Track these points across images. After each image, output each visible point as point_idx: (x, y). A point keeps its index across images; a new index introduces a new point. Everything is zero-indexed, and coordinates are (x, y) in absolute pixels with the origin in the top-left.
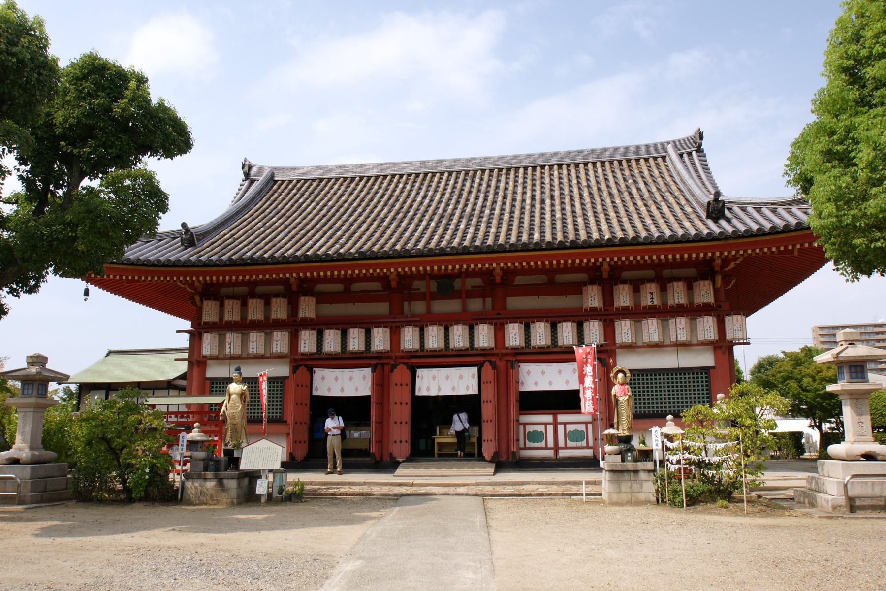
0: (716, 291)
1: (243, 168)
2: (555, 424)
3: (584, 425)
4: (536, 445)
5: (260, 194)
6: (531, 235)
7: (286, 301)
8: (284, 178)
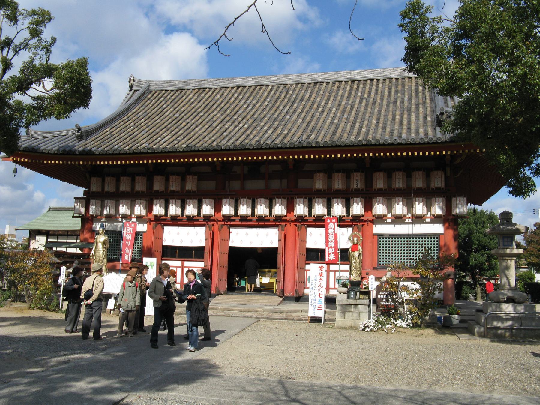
0: (446, 177)
1: (129, 82)
3: (330, 273)
5: (138, 99)
6: (417, 132)
7: (146, 178)
8: (156, 89)
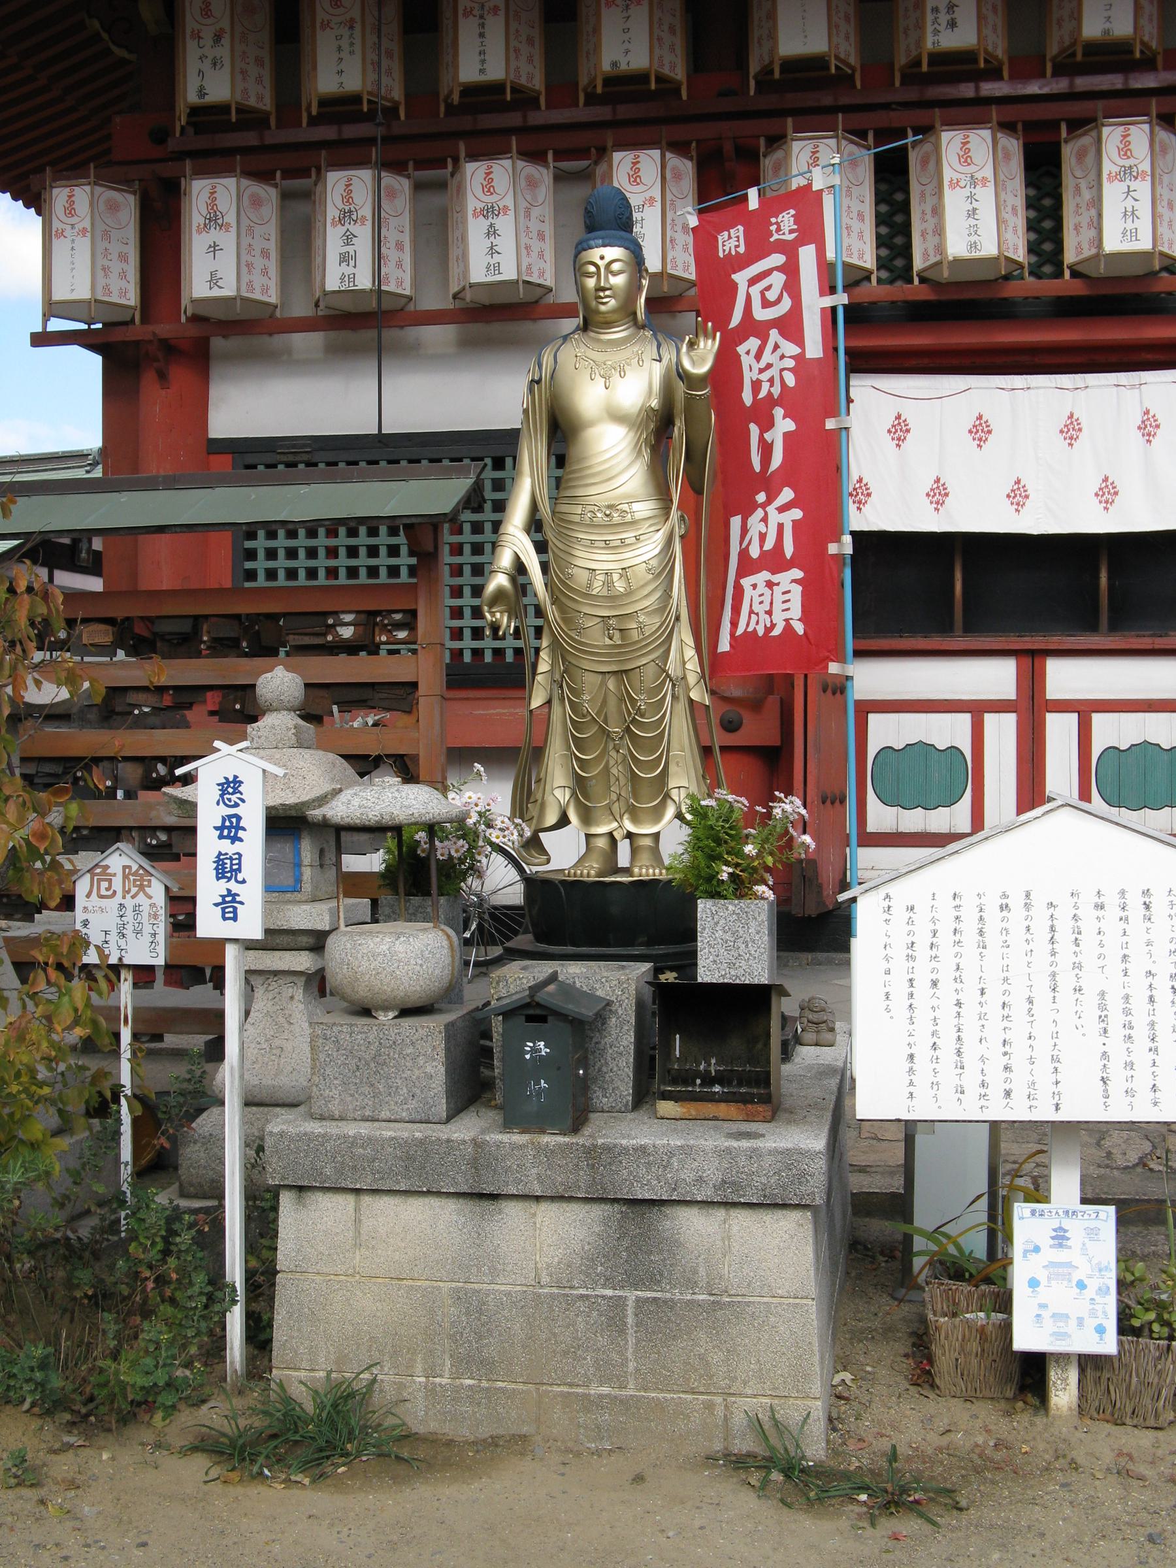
2: (1032, 707)
3: (965, 719)
4: (914, 820)
